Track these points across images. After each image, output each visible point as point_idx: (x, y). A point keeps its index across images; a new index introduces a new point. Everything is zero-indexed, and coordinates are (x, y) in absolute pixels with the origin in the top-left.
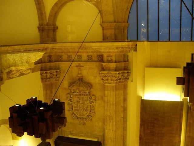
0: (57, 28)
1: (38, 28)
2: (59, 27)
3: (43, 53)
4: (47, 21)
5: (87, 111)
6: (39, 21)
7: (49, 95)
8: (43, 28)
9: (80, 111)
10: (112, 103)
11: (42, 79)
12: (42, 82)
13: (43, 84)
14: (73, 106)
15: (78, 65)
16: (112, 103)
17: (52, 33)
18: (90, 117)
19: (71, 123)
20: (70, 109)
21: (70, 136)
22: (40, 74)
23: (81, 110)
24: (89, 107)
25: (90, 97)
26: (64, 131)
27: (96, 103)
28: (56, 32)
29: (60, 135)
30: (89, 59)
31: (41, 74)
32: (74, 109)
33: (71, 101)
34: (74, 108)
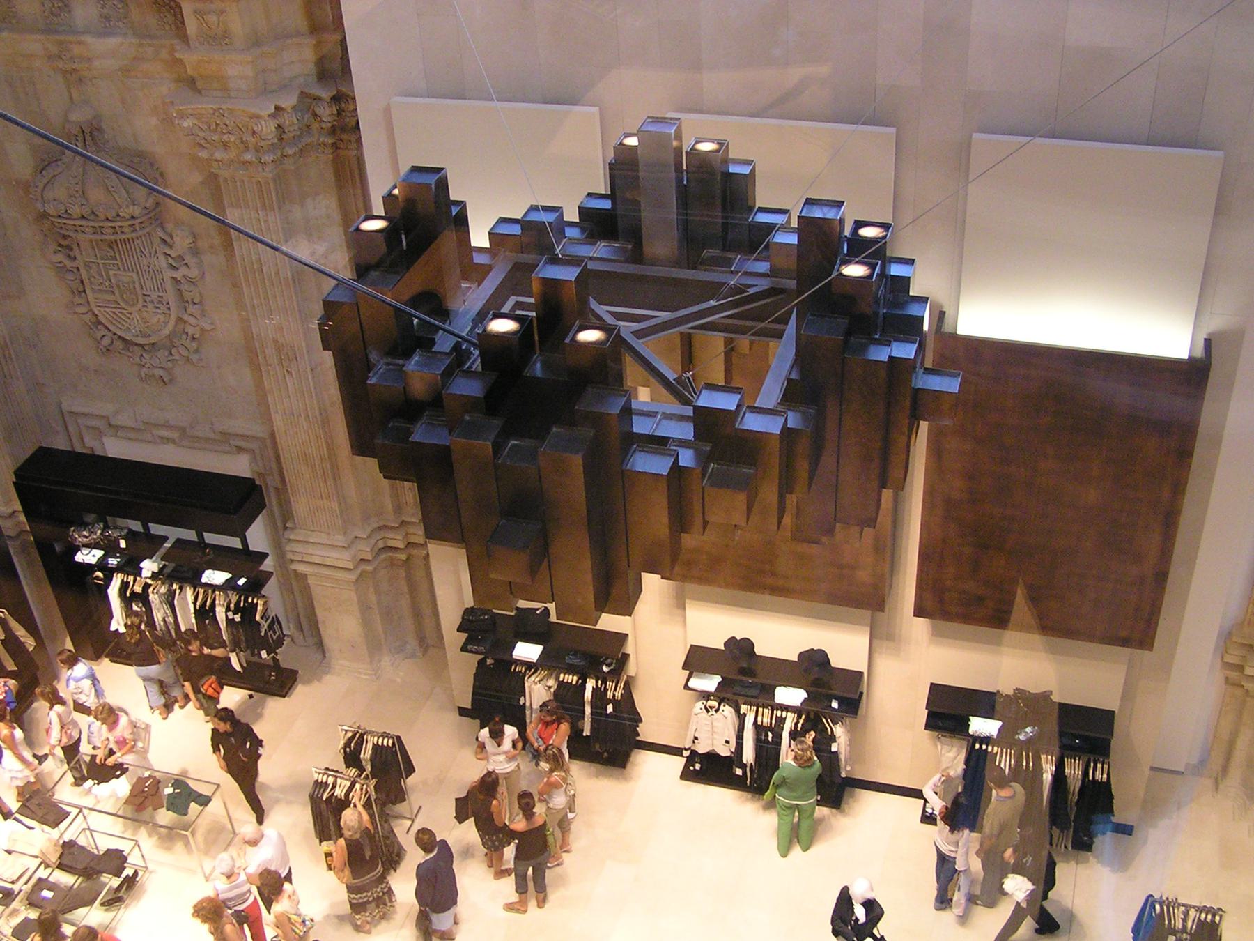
24: (169, 285)
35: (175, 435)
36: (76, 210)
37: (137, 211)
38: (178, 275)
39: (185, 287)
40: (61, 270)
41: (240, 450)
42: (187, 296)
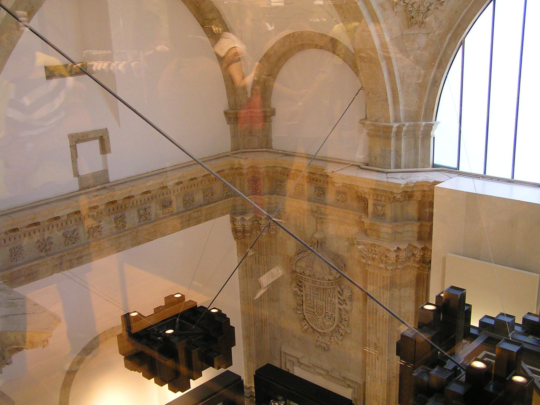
0: (273, 113)
1: (226, 113)
2: (277, 111)
3: (244, 378)
4: (249, 95)
5: (332, 320)
6: (229, 97)
7: (252, 269)
8: (236, 113)
9: (319, 317)
10: (383, 316)
11: (235, 231)
12: (236, 238)
13: (237, 243)
14: (304, 300)
15: (315, 209)
16: (383, 316)
17: (261, 124)
18: (338, 336)
19: (299, 339)
20: (299, 308)
21: (298, 372)
22: (231, 221)
23: (320, 315)
24: (337, 310)
25: (339, 289)
26: (285, 353)
27: (351, 305)
28: (271, 121)
29: (277, 364)
30: (338, 201)
31: (233, 221)
32: (306, 309)
33: (300, 290)
34: (306, 305)
35: (324, 373)
36: (307, 273)
37: (331, 278)
38: (342, 307)
39: (343, 313)
40: (295, 294)
41: (349, 386)
42: (343, 317)
